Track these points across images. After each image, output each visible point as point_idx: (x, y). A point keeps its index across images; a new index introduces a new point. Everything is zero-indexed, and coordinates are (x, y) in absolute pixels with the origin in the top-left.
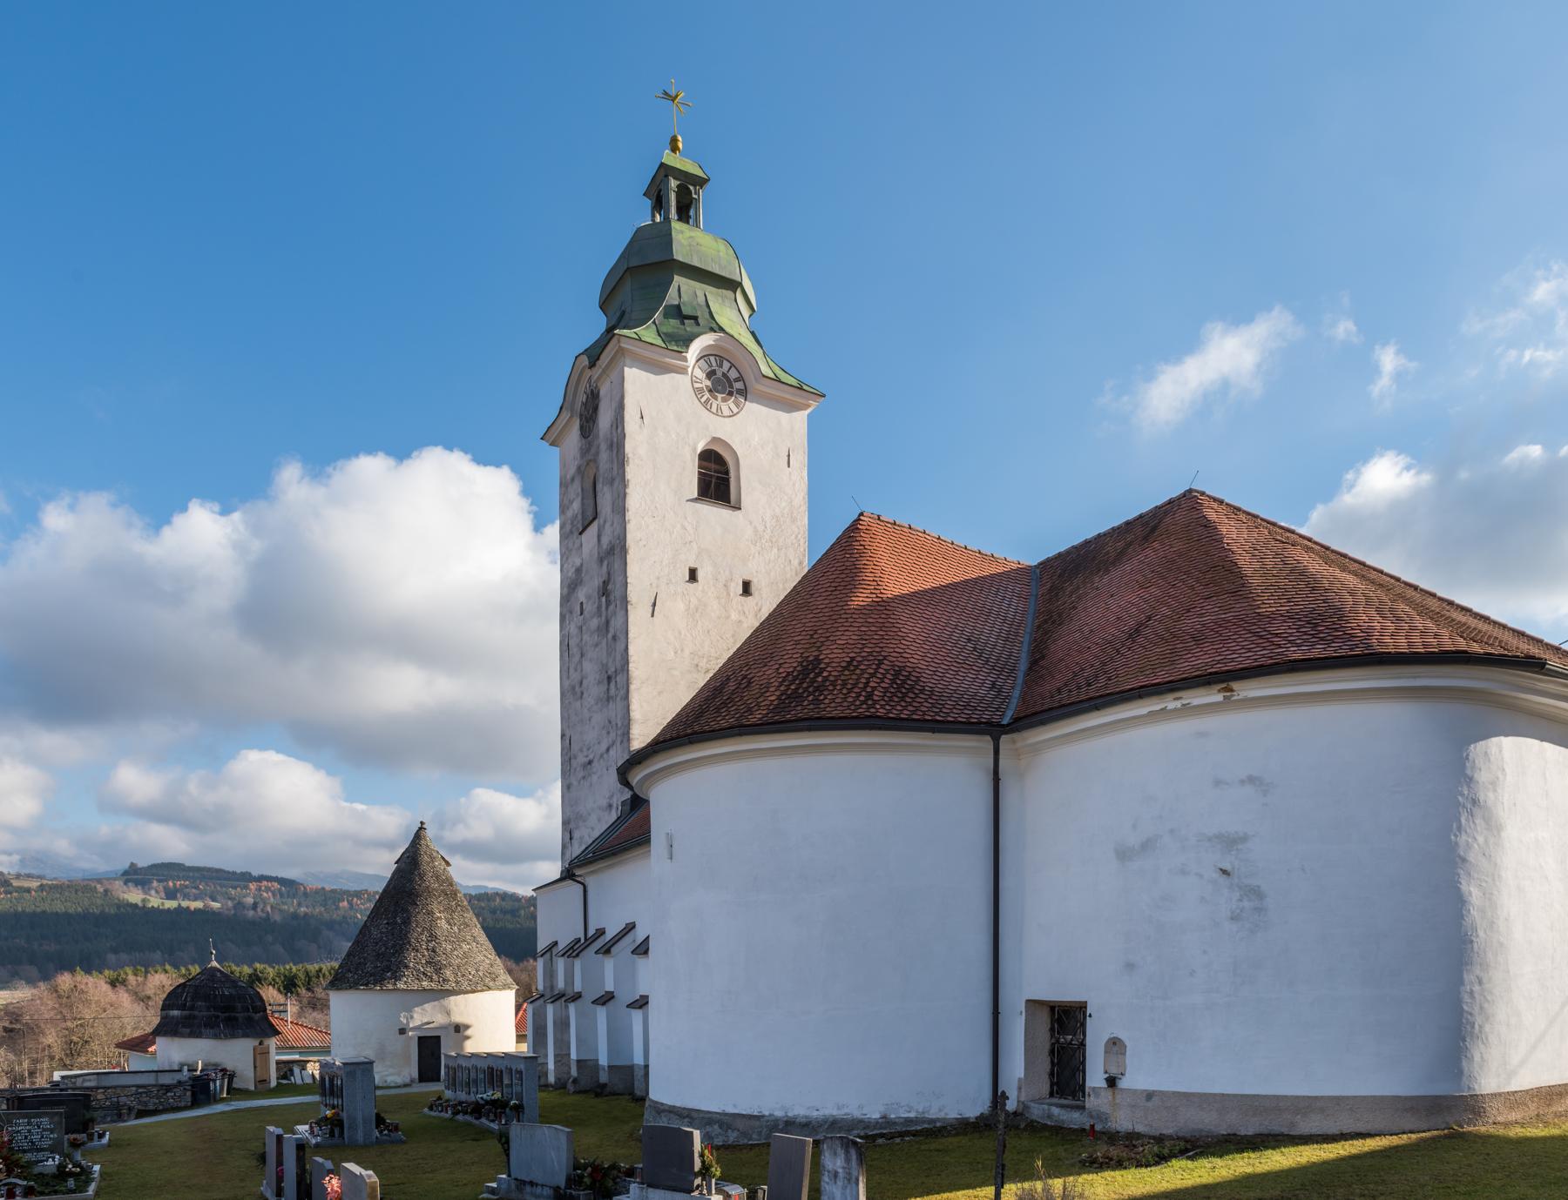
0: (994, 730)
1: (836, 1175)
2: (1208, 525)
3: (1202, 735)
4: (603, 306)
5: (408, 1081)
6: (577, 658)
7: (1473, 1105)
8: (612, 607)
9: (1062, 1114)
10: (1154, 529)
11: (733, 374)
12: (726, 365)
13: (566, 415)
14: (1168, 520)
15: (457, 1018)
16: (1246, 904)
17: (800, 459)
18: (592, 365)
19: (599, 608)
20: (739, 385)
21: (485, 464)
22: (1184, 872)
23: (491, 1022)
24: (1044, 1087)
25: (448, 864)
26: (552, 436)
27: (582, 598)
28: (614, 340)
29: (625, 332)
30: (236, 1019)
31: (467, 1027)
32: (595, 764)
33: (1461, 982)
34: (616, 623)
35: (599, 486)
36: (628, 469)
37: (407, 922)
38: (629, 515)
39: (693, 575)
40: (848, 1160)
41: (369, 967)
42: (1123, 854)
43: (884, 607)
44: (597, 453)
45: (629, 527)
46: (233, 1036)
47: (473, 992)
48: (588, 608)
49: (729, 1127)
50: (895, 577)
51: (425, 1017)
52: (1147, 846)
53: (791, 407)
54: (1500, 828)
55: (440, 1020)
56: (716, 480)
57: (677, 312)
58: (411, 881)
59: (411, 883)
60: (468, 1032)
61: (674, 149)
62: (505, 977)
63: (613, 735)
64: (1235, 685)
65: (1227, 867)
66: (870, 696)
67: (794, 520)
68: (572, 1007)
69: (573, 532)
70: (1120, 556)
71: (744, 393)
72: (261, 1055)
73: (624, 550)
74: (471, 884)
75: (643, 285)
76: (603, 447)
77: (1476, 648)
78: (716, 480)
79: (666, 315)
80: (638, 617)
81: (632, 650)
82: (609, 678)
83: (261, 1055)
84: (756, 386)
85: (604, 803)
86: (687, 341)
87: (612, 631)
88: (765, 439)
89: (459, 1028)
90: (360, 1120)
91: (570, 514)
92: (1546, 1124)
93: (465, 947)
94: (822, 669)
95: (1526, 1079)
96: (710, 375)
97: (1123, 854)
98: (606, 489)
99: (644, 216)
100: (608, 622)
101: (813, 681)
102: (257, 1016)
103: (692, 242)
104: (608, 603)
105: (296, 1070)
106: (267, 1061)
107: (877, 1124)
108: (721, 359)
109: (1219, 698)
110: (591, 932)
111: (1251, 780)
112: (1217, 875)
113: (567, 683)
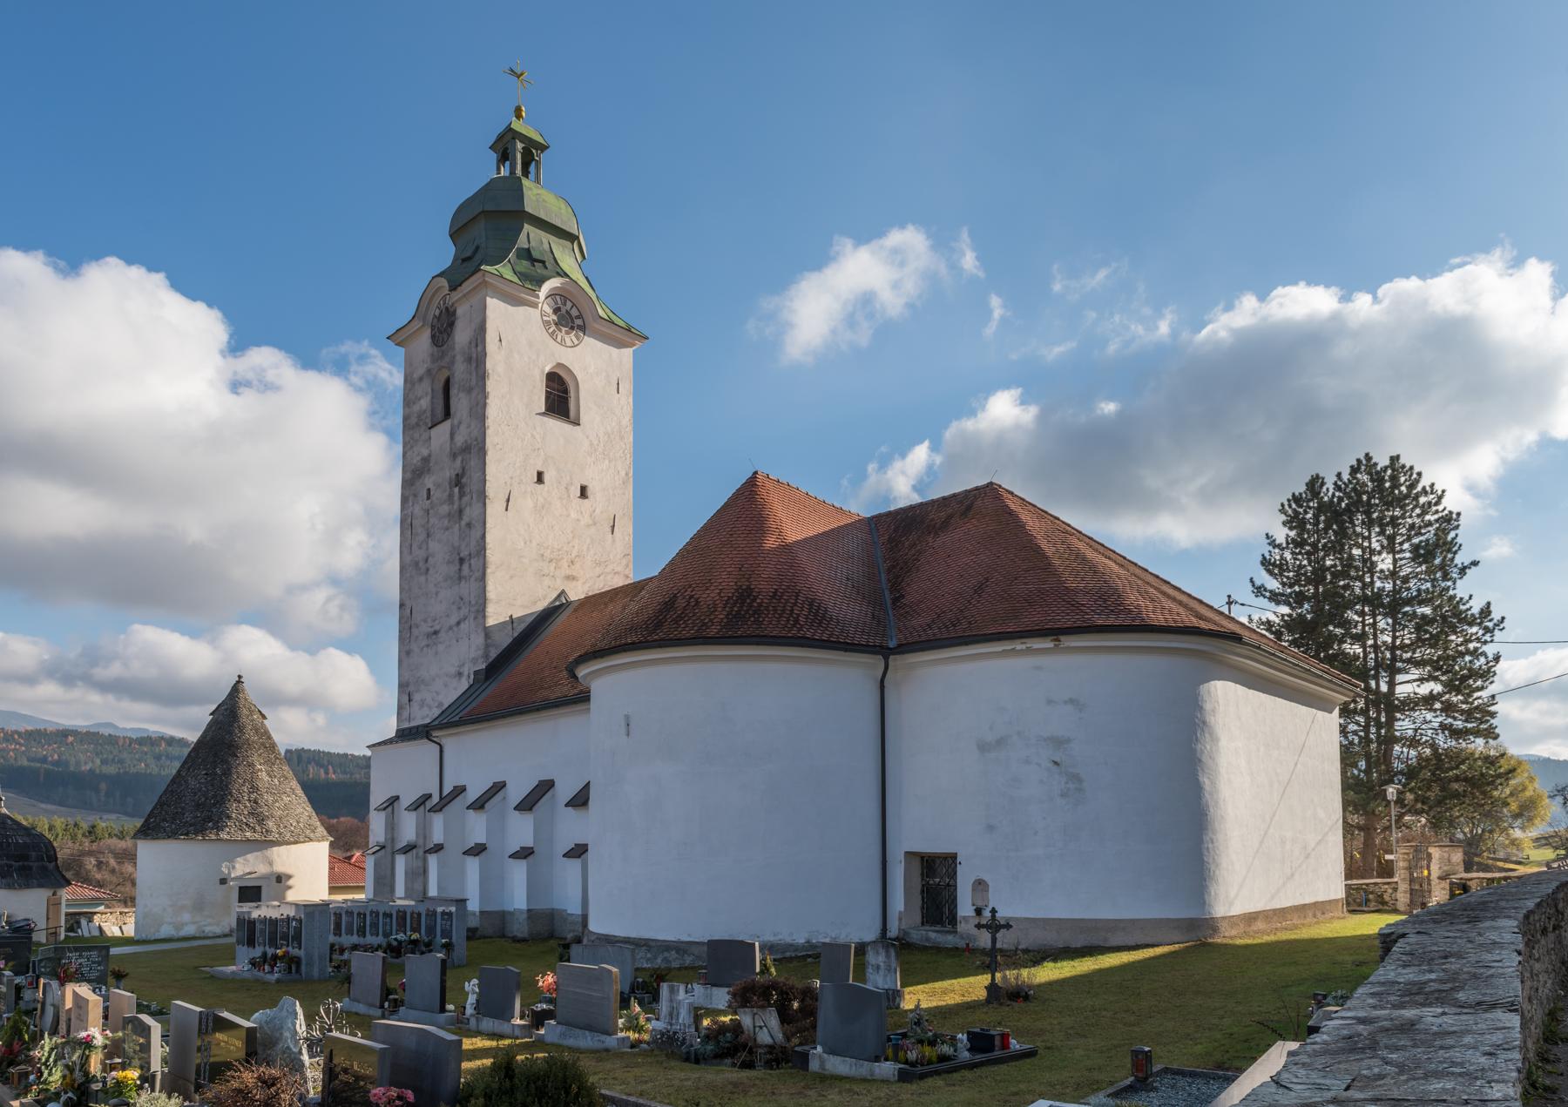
0: (885, 652)
1: (878, 967)
2: (1011, 513)
3: (1038, 668)
4: (454, 235)
5: (227, 930)
6: (422, 537)
7: (1211, 925)
8: (466, 499)
9: (934, 936)
10: (969, 508)
11: (574, 312)
12: (569, 304)
13: (417, 324)
14: (979, 502)
15: (279, 868)
16: (1071, 786)
17: (627, 387)
18: (453, 288)
19: (451, 496)
20: (579, 322)
21: (194, 299)
22: (1027, 762)
23: (307, 871)
24: (917, 918)
25: (264, 717)
26: (399, 337)
27: (430, 485)
28: (479, 275)
29: (488, 268)
30: (30, 868)
31: (289, 877)
32: (442, 634)
33: (1201, 841)
34: (471, 513)
35: (453, 392)
36: (488, 383)
37: (227, 773)
38: (489, 422)
39: (540, 478)
40: (888, 956)
41: (188, 817)
42: (983, 747)
43: (787, 549)
44: (452, 363)
45: (489, 432)
46: (28, 886)
47: (296, 843)
48: (436, 494)
49: (685, 952)
50: (793, 527)
51: (246, 866)
52: (1001, 742)
53: (620, 345)
54: (1218, 740)
55: (262, 869)
56: (559, 398)
57: (526, 254)
58: (230, 733)
59: (229, 731)
60: (290, 882)
61: (519, 116)
62: (321, 830)
63: (464, 611)
64: (1062, 638)
65: (1057, 759)
66: (796, 621)
67: (622, 438)
68: (433, 860)
69: (415, 427)
70: (946, 524)
71: (583, 328)
72: (53, 905)
73: (482, 452)
74: (129, 726)
75: (491, 230)
76: (459, 359)
77: (1203, 625)
78: (559, 398)
79: (519, 256)
80: (494, 510)
81: (490, 538)
82: (462, 561)
83: (53, 905)
84: (593, 324)
85: (453, 670)
86: (540, 282)
87: (466, 519)
88: (596, 365)
89: (280, 878)
90: (316, 957)
91: (416, 408)
92: (1250, 936)
93: (286, 799)
94: (733, 589)
95: (1237, 909)
96: (556, 311)
97: (983, 747)
98: (462, 395)
99: (487, 170)
100: (461, 511)
101: (750, 606)
102: (51, 866)
103: (538, 197)
104: (462, 494)
105: (84, 922)
106: (59, 911)
107: (803, 947)
108: (565, 299)
109: (1051, 645)
110: (447, 789)
111: (1071, 701)
112: (1051, 765)
113: (408, 559)
